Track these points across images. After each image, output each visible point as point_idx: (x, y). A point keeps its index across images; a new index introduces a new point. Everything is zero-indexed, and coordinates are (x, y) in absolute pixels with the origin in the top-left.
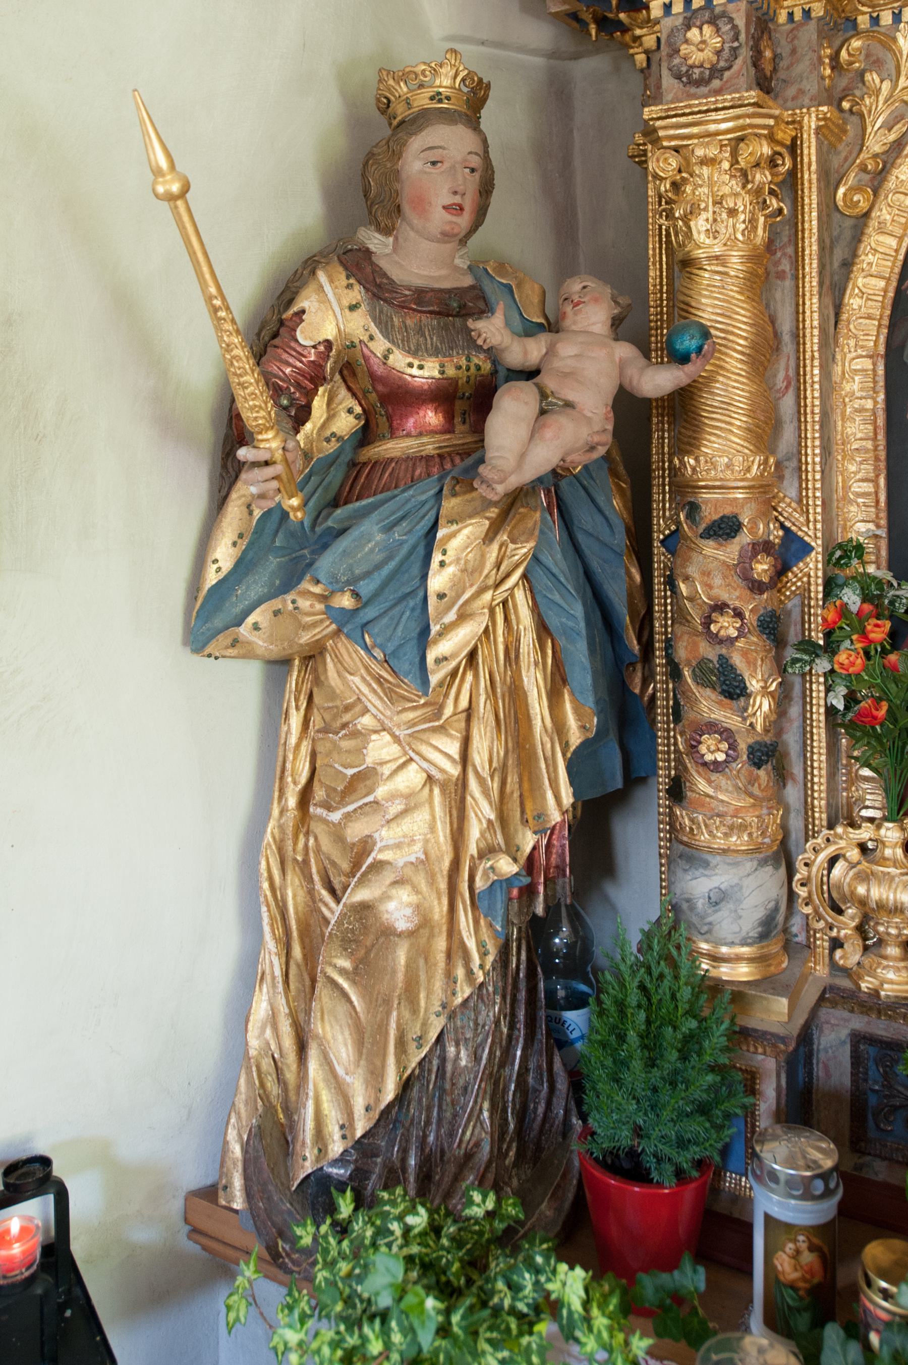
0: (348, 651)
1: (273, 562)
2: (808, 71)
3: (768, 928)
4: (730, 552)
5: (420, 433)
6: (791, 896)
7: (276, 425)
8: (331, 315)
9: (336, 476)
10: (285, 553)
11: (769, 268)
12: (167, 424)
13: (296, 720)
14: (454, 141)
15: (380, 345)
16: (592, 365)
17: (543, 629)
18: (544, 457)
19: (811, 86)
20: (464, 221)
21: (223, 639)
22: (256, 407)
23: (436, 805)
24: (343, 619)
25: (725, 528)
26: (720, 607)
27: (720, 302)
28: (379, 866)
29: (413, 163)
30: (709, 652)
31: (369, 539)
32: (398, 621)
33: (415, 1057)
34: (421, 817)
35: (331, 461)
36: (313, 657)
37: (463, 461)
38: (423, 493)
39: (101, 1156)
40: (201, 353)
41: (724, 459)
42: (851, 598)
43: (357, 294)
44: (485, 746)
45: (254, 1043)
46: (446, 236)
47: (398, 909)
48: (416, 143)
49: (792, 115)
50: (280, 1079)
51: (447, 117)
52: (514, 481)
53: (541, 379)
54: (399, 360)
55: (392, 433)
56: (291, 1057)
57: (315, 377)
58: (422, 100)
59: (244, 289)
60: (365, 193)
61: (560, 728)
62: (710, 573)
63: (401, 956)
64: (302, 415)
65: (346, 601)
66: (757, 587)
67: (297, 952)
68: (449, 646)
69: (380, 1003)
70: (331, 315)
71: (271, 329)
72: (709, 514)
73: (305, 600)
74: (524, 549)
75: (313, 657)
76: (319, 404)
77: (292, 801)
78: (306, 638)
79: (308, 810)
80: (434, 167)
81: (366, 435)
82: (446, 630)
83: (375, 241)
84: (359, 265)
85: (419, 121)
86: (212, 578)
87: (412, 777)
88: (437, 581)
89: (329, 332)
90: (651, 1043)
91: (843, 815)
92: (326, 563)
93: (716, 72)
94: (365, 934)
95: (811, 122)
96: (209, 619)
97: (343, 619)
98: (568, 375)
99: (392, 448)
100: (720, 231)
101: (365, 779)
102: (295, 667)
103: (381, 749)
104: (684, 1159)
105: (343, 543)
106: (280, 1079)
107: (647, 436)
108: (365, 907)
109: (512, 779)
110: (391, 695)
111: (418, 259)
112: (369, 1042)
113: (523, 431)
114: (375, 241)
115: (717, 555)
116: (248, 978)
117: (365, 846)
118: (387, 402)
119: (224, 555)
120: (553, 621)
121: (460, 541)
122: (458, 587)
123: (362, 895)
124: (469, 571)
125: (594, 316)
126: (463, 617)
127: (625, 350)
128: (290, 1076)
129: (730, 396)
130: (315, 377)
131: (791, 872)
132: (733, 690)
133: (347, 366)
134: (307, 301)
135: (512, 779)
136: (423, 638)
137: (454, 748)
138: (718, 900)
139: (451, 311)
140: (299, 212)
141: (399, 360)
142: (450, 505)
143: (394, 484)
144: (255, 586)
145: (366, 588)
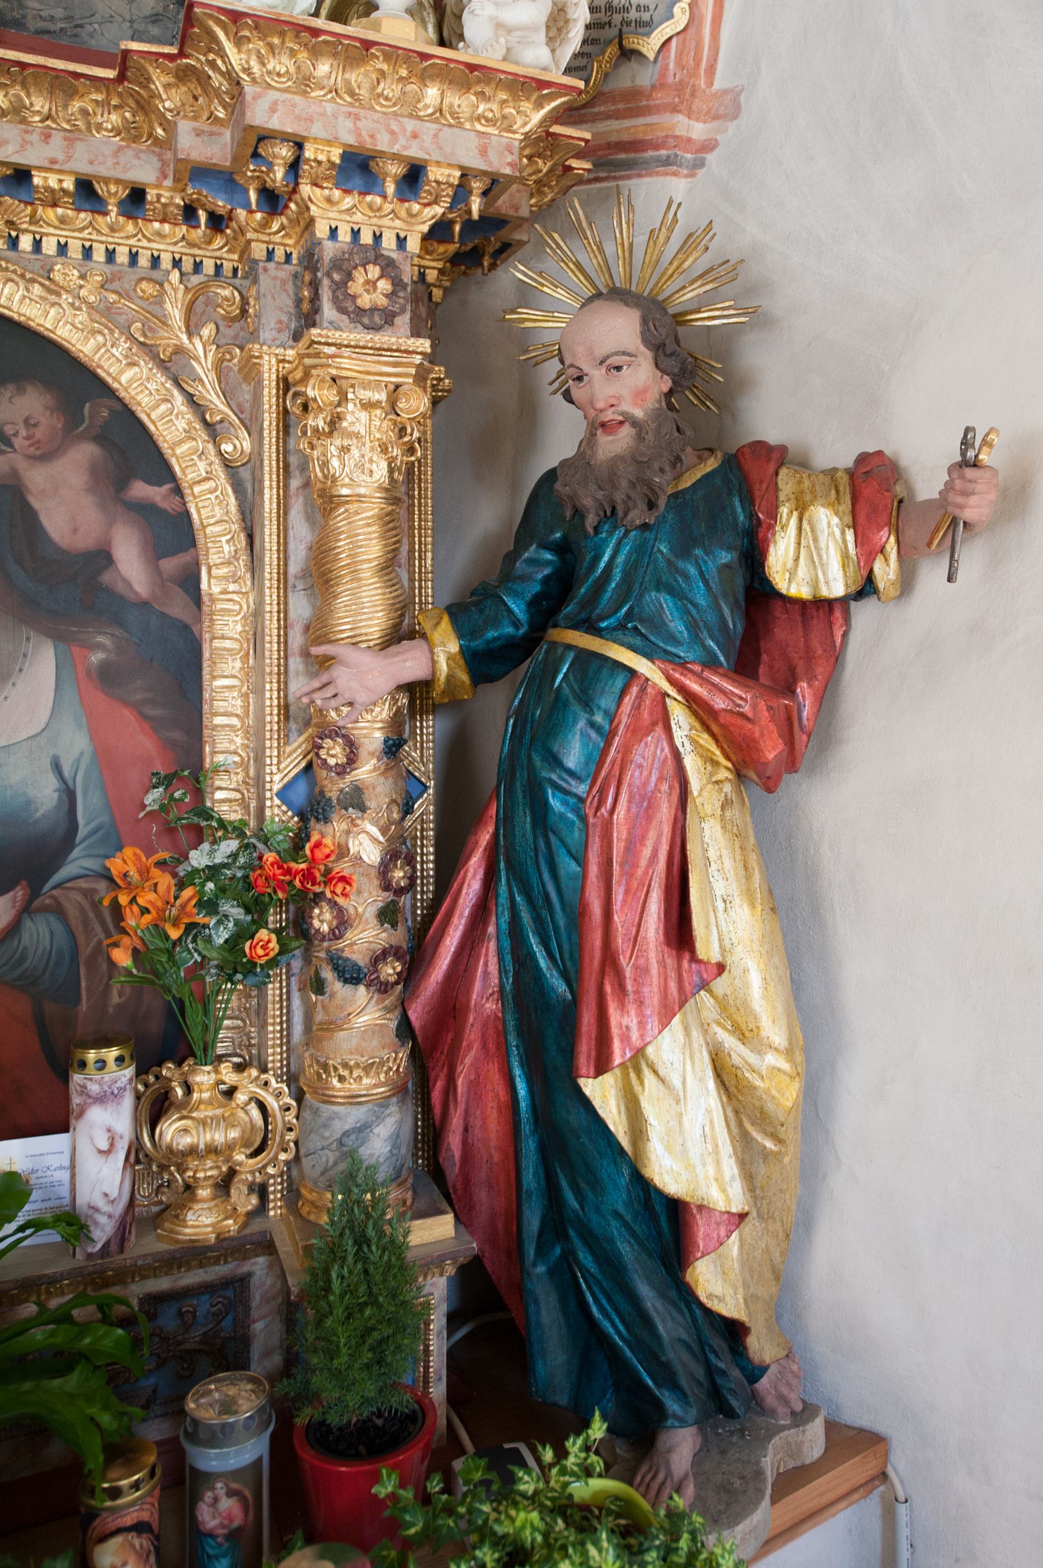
57: (776, 1388)
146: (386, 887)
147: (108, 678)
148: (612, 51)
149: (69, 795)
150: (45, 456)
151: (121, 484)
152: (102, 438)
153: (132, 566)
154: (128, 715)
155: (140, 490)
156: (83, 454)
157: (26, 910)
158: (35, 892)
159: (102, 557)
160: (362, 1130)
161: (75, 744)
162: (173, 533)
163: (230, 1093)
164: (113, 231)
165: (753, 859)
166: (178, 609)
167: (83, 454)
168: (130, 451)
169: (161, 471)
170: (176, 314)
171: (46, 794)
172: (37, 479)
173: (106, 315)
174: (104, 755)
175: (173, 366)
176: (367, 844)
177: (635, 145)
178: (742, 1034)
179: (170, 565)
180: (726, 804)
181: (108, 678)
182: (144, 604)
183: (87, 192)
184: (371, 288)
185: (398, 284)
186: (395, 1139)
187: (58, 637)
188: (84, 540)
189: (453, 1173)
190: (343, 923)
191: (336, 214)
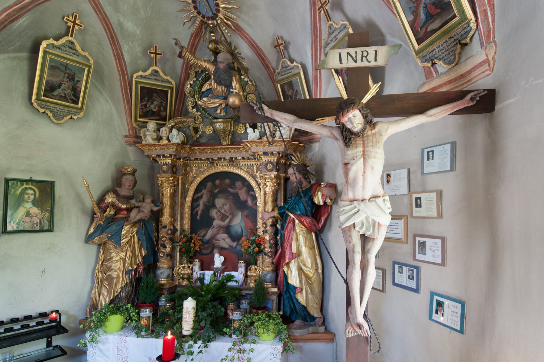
0: (110, 242)
1: (100, 231)
2: (181, 171)
3: (168, 277)
4: (165, 230)
5: (123, 214)
6: (173, 274)
7: (100, 213)
8: (110, 199)
9: (110, 220)
10: (100, 230)
11: (173, 196)
12: (84, 211)
13: (101, 253)
14: (130, 178)
15: (117, 203)
16: (147, 207)
17: (139, 240)
18: (138, 217)
19: (181, 173)
20: (131, 187)
21: (91, 241)
22: (97, 210)
23: (122, 261)
24: (109, 238)
25: (165, 227)
26: (163, 237)
27: (167, 200)
28: (112, 269)
29: (124, 179)
30: (162, 242)
31: (114, 227)
32: (117, 238)
33: (116, 294)
34: (119, 263)
35: (110, 217)
36: (105, 244)
37: (127, 219)
38: (122, 222)
39: (67, 313)
40: (90, 204)
41: (166, 218)
42: (182, 236)
43: (114, 196)
44: (129, 254)
45: (92, 296)
46: (128, 189)
47: (114, 275)
48: (124, 177)
49: (199, 168)
50: (96, 301)
51: (129, 174)
52: (134, 220)
53: (140, 208)
54: (120, 205)
55: (119, 214)
56: (98, 297)
57: (108, 206)
58: (126, 172)
59: (96, 196)
60: (117, 181)
61: (141, 253)
62: (163, 233)
63: (115, 281)
64: (105, 211)
65: (110, 235)
66: (168, 234)
67: (100, 283)
68: (124, 241)
69: (111, 287)
70: (110, 199)
71: (101, 200)
72: (163, 225)
73: (104, 236)
74: (135, 229)
75: (105, 244)
76: (108, 210)
77: (100, 263)
78: (103, 241)
79: (104, 266)
80: (127, 181)
81: (115, 214)
82: (124, 239)
83: (118, 189)
84: (115, 192)
85: (124, 174)
86: (90, 233)
87: (118, 258)
88: (123, 233)
89: (110, 201)
90: (147, 287)
91: (181, 263)
92: (107, 230)
93: (166, 171)
94: (110, 279)
95: (180, 178)
96: (89, 239)
97: (109, 238)
98: (143, 208)
99: (119, 216)
100: (167, 191)
101: (111, 258)
102: (102, 245)
103: (113, 254)
104: (150, 301)
105: (110, 228)
106: (96, 301)
107: (156, 216)
108: (110, 275)
109: (133, 259)
110: (116, 248)
111: (124, 191)
112: (109, 292)
113: (135, 214)
114: (118, 189)
115: (165, 230)
116: (92, 288)
117: (111, 267)
118: (118, 210)
119: (92, 230)
120: (141, 239)
121: (126, 228)
122: (126, 233)
123: (109, 273)
124: (128, 232)
125: (148, 200)
126: (126, 237)
127: (152, 205)
128: (98, 300)
129: (167, 212)
130: (108, 206)
131: (173, 270)
132: (165, 247)
133: (113, 205)
134: (107, 197)
135: (133, 259)
136: (120, 240)
137: (124, 254)
138: (161, 273)
139: (128, 199)
140: (109, 183)
141: (120, 205)
142: (125, 223)
143: (119, 220)
144: (97, 234)
145: (112, 234)
146: (270, 243)
147: (247, 216)
148: (459, 46)
149: (242, 231)
150: (241, 189)
151: (249, 192)
152: (247, 187)
153: (250, 202)
154: (249, 221)
155: (251, 193)
156: (245, 188)
157: (237, 244)
158: (238, 242)
159: (246, 201)
160: (266, 274)
161: (243, 224)
162: (254, 198)
163: (256, 269)
164: (247, 162)
165: (308, 242)
166: (255, 208)
167: (245, 188)
168: (250, 188)
169: (253, 190)
170: (255, 171)
171: (240, 230)
172: (240, 192)
173: (247, 172)
174: (246, 226)
175: (254, 177)
176: (267, 237)
177: (312, 139)
178: (305, 265)
179: (254, 202)
180: (304, 233)
181: (247, 216)
182: (251, 207)
183: (243, 158)
184: (270, 166)
185: (273, 166)
186: (271, 277)
187: (241, 211)
188: (244, 199)
189: (279, 283)
190: (265, 248)
191: (265, 159)
